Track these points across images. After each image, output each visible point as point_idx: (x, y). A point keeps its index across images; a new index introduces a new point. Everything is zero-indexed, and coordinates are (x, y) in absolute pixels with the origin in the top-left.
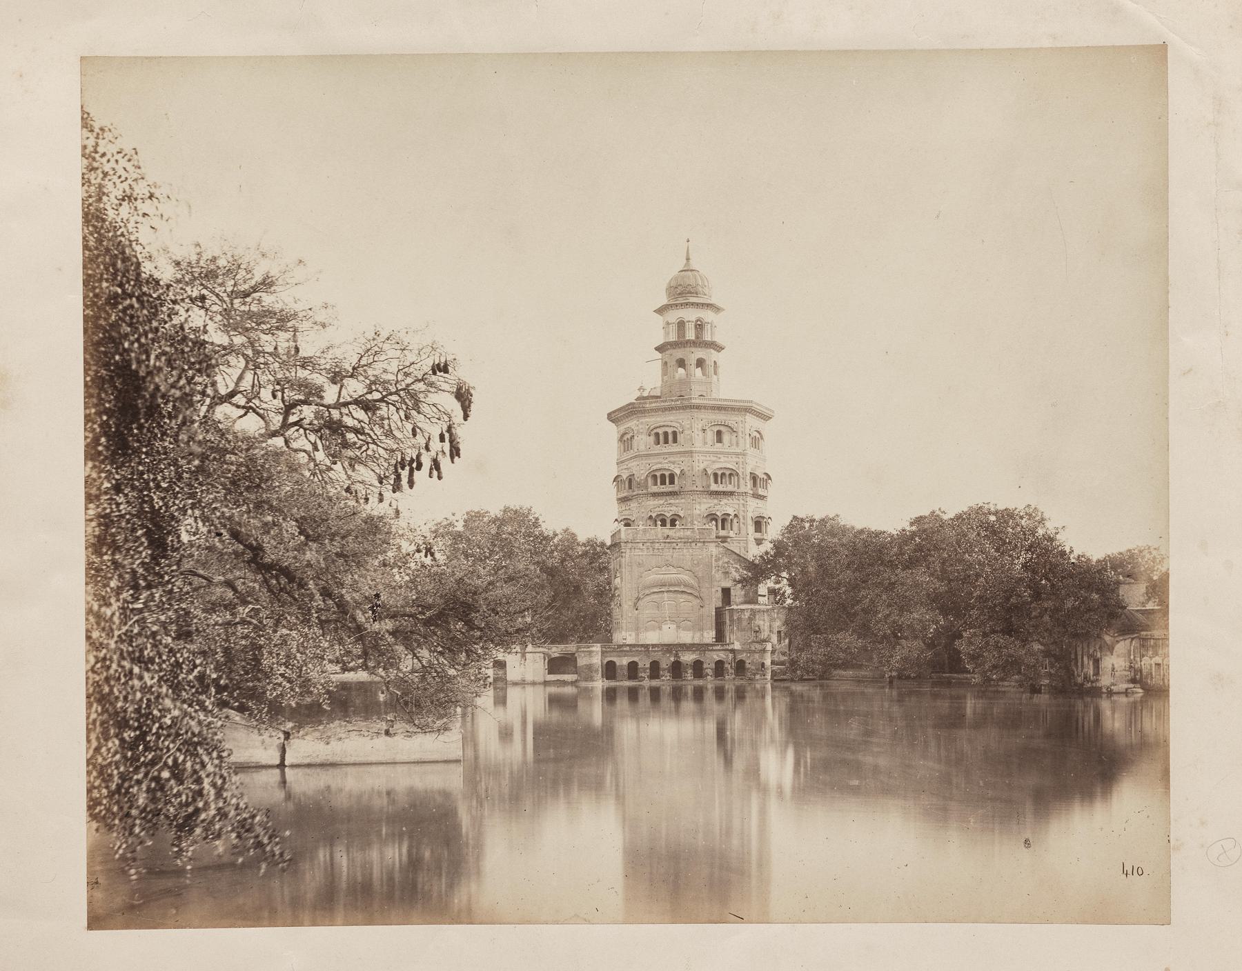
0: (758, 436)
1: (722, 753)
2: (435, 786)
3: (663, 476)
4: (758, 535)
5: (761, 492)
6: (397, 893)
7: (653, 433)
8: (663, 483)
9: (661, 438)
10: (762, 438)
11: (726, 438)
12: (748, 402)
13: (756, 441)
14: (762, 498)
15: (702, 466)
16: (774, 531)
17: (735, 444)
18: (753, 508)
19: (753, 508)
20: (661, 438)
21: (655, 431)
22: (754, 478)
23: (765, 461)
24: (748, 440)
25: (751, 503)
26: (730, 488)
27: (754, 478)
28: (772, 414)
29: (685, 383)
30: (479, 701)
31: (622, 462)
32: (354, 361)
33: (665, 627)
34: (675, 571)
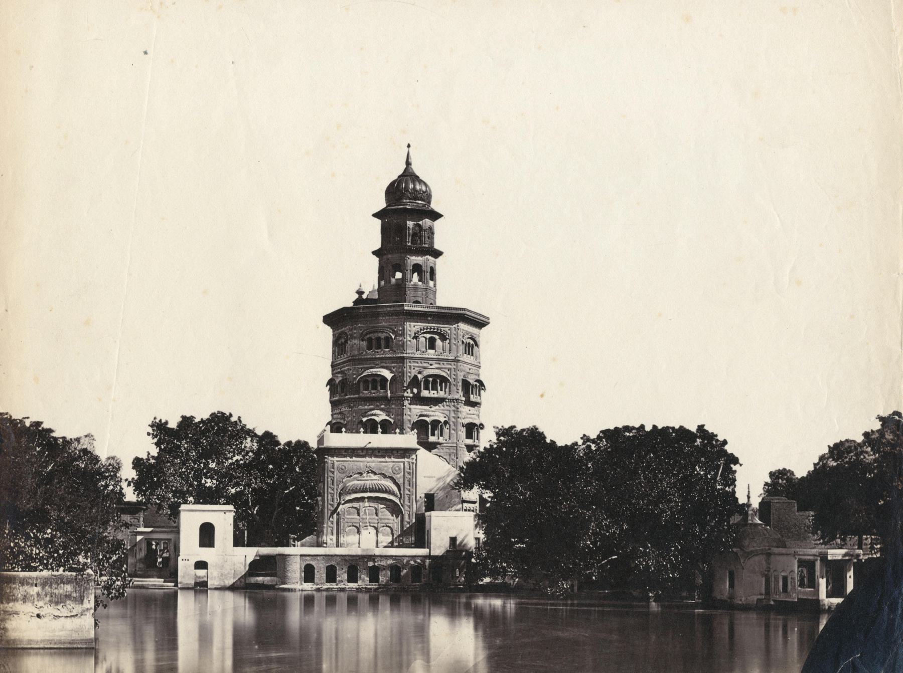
0: (472, 342)
1: (763, 623)
2: (128, 631)
3: (374, 381)
4: (470, 442)
5: (473, 398)
6: (430, 386)
7: (366, 338)
8: (375, 388)
9: (374, 342)
10: (477, 345)
11: (439, 343)
12: (460, 309)
13: (471, 347)
14: (475, 404)
15: (414, 372)
16: (487, 439)
17: (447, 350)
18: (467, 414)
19: (467, 414)
20: (374, 342)
21: (368, 336)
22: (466, 385)
23: (479, 367)
24: (461, 348)
25: (464, 410)
26: (441, 394)
27: (466, 385)
28: (487, 320)
29: (401, 287)
30: (208, 486)
31: (337, 365)
32: (146, 457)
33: (364, 532)
34: (376, 477)
